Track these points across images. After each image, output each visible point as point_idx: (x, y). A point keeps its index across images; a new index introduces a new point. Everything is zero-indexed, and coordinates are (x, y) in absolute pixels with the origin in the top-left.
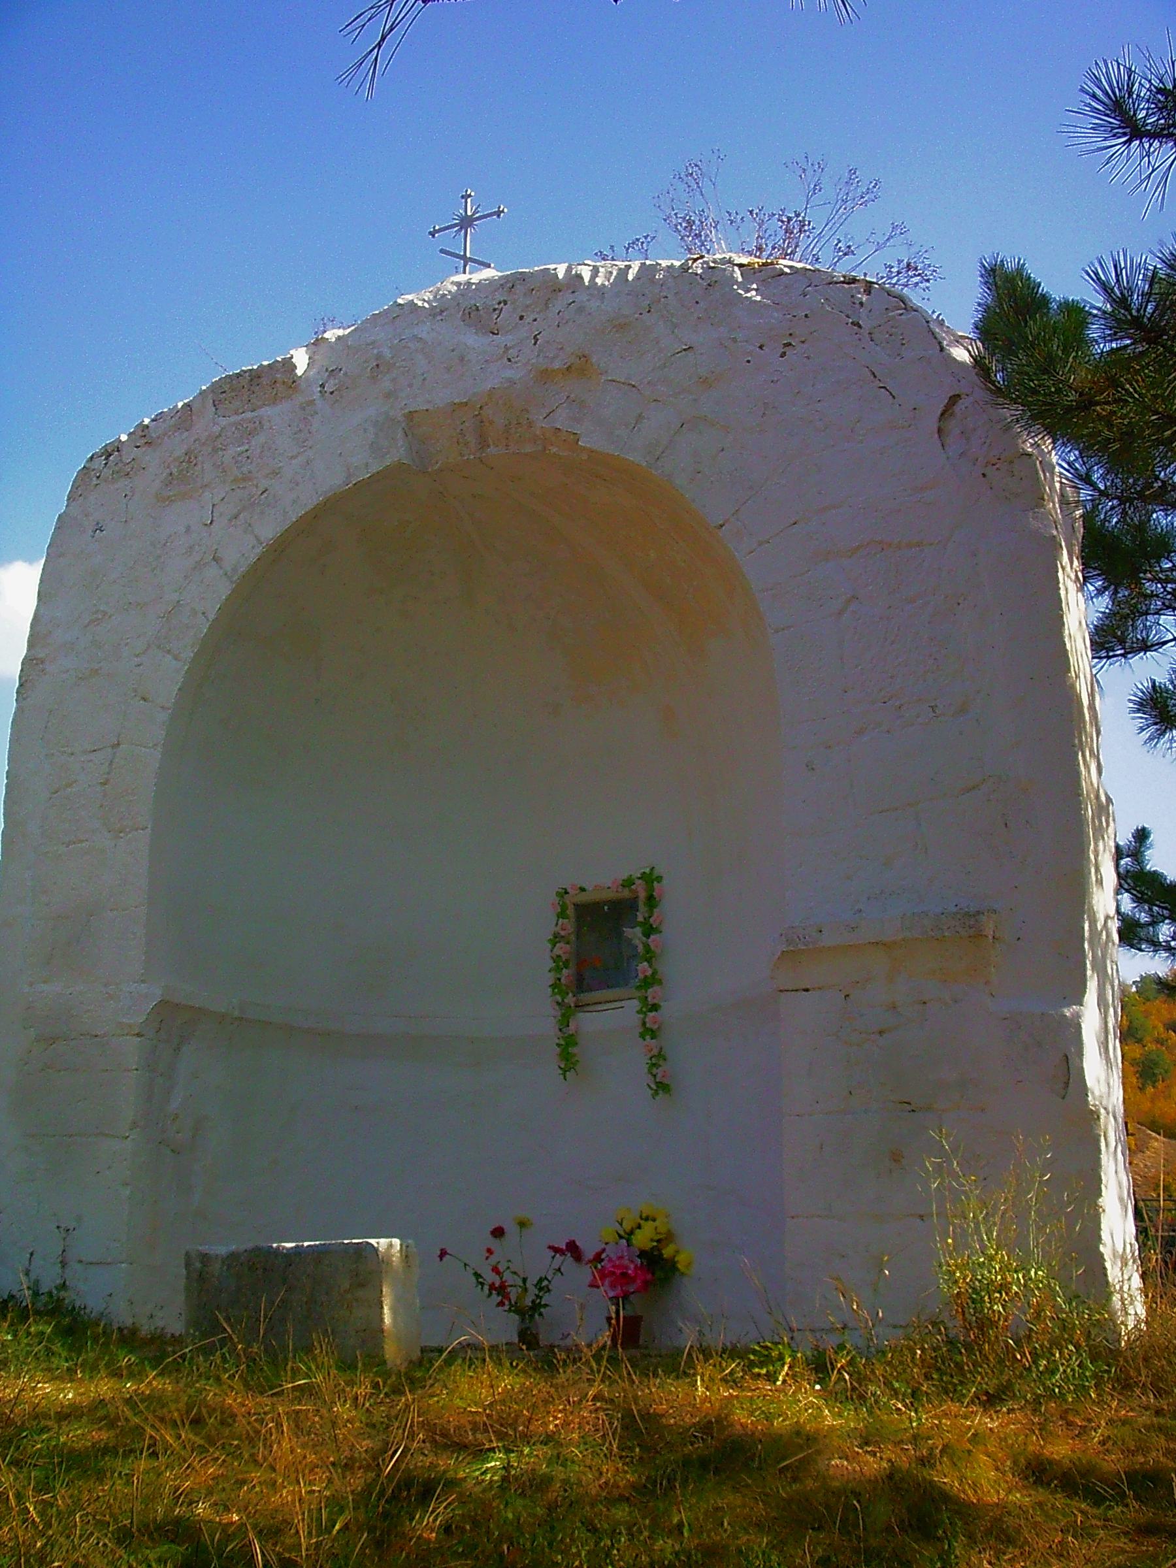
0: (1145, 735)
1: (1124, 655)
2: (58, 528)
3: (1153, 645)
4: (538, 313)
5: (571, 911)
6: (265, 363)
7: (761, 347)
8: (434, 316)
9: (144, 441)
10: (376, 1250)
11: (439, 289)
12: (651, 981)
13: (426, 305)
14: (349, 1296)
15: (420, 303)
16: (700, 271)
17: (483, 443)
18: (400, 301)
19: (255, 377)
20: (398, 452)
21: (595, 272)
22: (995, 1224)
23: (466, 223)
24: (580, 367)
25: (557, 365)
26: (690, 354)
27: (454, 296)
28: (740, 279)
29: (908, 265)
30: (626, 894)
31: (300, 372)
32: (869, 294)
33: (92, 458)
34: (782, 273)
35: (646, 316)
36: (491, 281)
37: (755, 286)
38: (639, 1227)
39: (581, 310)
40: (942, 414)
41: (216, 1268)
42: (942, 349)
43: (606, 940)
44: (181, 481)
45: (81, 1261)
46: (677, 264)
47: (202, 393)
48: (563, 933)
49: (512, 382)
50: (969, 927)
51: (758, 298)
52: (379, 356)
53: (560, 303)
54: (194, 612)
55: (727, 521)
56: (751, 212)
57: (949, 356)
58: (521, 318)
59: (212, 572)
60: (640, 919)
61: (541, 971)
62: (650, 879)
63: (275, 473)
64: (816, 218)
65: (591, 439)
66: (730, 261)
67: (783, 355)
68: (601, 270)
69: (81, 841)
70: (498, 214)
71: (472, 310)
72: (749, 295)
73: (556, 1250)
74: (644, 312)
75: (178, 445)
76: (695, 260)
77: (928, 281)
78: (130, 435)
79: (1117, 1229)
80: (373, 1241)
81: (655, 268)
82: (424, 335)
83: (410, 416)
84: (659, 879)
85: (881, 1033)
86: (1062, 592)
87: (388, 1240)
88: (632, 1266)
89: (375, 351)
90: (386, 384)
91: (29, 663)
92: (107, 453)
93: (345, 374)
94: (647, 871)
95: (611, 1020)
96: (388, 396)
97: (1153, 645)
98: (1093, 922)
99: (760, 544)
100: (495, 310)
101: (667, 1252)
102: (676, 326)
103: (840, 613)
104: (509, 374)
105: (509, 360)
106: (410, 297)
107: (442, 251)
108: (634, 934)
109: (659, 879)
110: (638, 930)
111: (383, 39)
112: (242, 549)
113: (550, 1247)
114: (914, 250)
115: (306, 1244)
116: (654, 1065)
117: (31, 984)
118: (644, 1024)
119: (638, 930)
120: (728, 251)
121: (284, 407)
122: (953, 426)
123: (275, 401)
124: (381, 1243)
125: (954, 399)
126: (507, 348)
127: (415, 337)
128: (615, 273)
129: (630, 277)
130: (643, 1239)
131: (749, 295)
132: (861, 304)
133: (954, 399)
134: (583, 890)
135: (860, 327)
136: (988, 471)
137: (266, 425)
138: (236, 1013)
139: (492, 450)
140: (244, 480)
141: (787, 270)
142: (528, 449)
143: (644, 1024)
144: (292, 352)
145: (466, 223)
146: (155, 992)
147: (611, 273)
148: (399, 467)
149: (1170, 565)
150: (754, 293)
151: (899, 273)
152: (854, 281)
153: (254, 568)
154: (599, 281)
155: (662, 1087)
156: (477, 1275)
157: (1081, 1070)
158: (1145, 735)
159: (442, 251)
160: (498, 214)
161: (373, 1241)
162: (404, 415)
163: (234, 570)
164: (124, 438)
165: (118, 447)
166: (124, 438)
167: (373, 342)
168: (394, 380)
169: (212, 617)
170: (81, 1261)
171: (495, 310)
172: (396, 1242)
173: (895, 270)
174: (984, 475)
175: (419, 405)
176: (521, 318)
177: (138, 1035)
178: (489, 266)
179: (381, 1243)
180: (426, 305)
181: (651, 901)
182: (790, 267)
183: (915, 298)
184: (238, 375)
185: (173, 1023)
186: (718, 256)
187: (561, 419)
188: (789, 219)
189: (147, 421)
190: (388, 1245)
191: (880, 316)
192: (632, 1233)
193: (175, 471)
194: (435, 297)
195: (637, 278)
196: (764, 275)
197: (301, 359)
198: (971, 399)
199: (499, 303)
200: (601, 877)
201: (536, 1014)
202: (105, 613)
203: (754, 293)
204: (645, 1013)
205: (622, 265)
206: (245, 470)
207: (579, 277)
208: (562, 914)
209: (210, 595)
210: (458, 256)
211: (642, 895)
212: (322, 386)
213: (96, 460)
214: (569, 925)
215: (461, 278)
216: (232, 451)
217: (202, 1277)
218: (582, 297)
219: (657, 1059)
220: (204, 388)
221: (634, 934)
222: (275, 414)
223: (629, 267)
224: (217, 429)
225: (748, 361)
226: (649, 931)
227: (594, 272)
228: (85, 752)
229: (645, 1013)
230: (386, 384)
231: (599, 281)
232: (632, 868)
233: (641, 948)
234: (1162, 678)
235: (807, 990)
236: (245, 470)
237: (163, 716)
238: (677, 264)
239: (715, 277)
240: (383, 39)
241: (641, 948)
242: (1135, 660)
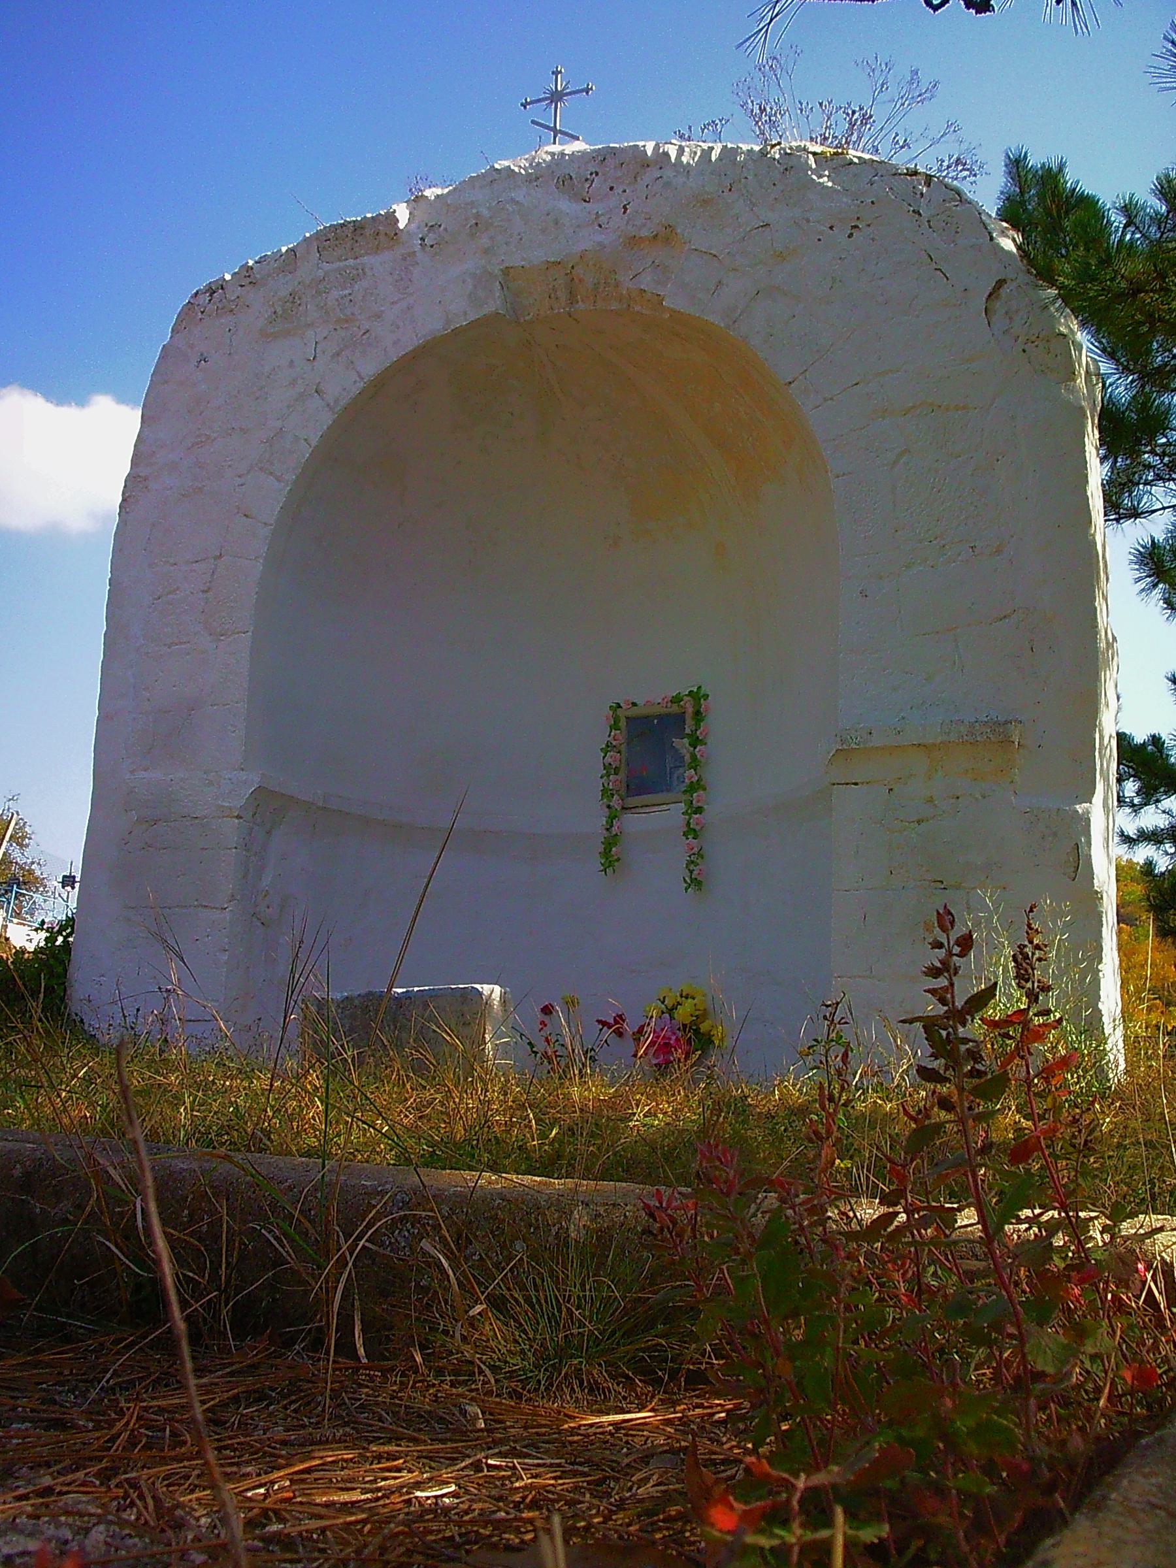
0: (1142, 585)
1: (1117, 520)
2: (163, 357)
3: (1143, 513)
5: (623, 723)
6: (369, 215)
7: (831, 228)
8: (530, 182)
9: (249, 280)
10: (481, 994)
11: (534, 158)
12: (695, 787)
13: (523, 172)
15: (516, 169)
16: (777, 156)
17: (572, 299)
18: (497, 166)
19: (358, 228)
20: (494, 304)
21: (681, 150)
22: (507, 1513)
23: (556, 97)
24: (666, 236)
25: (644, 233)
27: (549, 166)
28: (814, 166)
29: (958, 159)
30: (675, 709)
31: (401, 225)
32: (929, 186)
33: (196, 294)
34: (851, 163)
36: (584, 153)
37: (827, 173)
38: (679, 1004)
39: (667, 185)
40: (990, 296)
42: (992, 239)
43: (655, 749)
44: (285, 318)
46: (757, 148)
47: (306, 239)
48: (614, 743)
50: (997, 736)
51: (830, 184)
52: (478, 215)
53: (649, 176)
54: (297, 438)
56: (821, 104)
57: (998, 244)
58: (612, 189)
59: (316, 402)
60: (688, 731)
61: (594, 777)
63: (378, 316)
64: (879, 114)
65: (674, 301)
66: (805, 149)
67: (850, 236)
68: (687, 149)
69: (181, 643)
70: (587, 91)
71: (564, 177)
72: (821, 180)
73: (604, 1023)
74: (726, 190)
76: (773, 146)
77: (975, 175)
78: (234, 275)
79: (1110, 1000)
80: (478, 986)
81: (736, 151)
82: (520, 198)
83: (506, 271)
84: (706, 696)
85: (919, 822)
86: (1087, 455)
87: (491, 986)
88: (674, 1038)
89: (474, 211)
90: (485, 241)
91: (132, 482)
92: (211, 291)
93: (446, 230)
95: (656, 822)
96: (486, 251)
97: (1143, 513)
98: (1102, 738)
99: (825, 400)
100: (587, 180)
101: (704, 1027)
103: (895, 463)
104: (601, 238)
105: (600, 226)
106: (506, 163)
107: (533, 122)
108: (682, 745)
109: (706, 696)
110: (686, 741)
111: (771, 20)
112: (345, 382)
113: (599, 1021)
114: (964, 146)
115: (416, 989)
116: (693, 862)
117: (132, 772)
118: (688, 824)
119: (686, 741)
120: (793, 138)
121: (387, 256)
122: (998, 306)
123: (377, 250)
124: (485, 989)
125: (1000, 283)
127: (513, 200)
128: (699, 154)
129: (713, 159)
130: (684, 1013)
131: (821, 180)
132: (922, 194)
133: (1000, 283)
134: (634, 704)
135: (920, 214)
136: (1026, 347)
137: (369, 273)
138: (320, 804)
139: (581, 306)
141: (856, 160)
142: (615, 306)
143: (688, 824)
144: (394, 207)
145: (556, 97)
146: (253, 779)
147: (695, 153)
149: (1164, 440)
150: (826, 179)
151: (949, 167)
152: (915, 173)
154: (684, 159)
155: (695, 883)
157: (1089, 857)
158: (1142, 585)
159: (533, 122)
160: (587, 91)
161: (478, 986)
163: (337, 401)
164: (228, 277)
165: (222, 285)
166: (228, 277)
167: (472, 202)
168: (492, 238)
169: (314, 444)
171: (587, 180)
172: (497, 989)
173: (945, 164)
174: (1024, 351)
175: (516, 261)
176: (612, 189)
177: (238, 817)
178: (578, 139)
179: (485, 989)
180: (523, 172)
182: (859, 158)
183: (965, 187)
184: (342, 225)
185: (268, 808)
186: (794, 144)
187: (647, 281)
188: (854, 112)
189: (251, 263)
190: (493, 991)
191: (927, 200)
192: (674, 1008)
193: (279, 310)
194: (531, 165)
195: (720, 159)
196: (836, 162)
197: (402, 214)
198: (1015, 284)
200: (652, 691)
202: (208, 437)
203: (826, 179)
204: (690, 815)
205: (705, 146)
206: (348, 312)
207: (666, 154)
208: (615, 726)
209: (311, 425)
210: (547, 127)
211: (690, 710)
212: (422, 239)
213: (201, 296)
214: (621, 736)
215: (556, 148)
216: (335, 294)
218: (668, 173)
219: (696, 858)
220: (308, 235)
221: (682, 745)
222: (379, 263)
223: (712, 148)
224: (321, 273)
226: (696, 742)
227: (684, 152)
229: (690, 815)
230: (485, 241)
231: (684, 159)
232: (684, 688)
233: (687, 758)
234: (1160, 537)
235: (856, 784)
236: (348, 312)
238: (757, 148)
239: (791, 162)
240: (771, 20)
241: (687, 758)
242: (1127, 524)
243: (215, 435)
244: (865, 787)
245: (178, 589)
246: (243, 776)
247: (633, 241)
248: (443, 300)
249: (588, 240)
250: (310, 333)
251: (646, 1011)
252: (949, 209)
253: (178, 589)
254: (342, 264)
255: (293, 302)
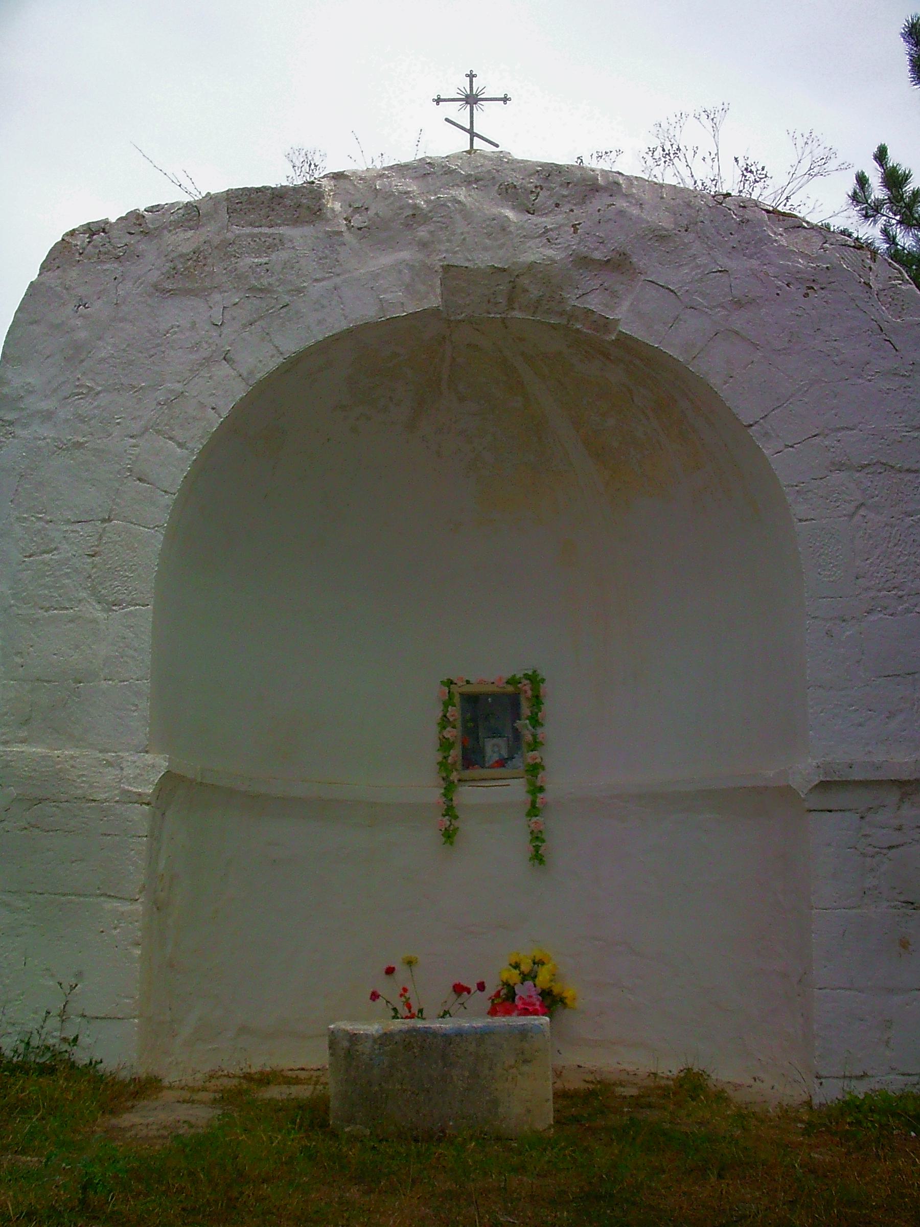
4: (575, 205)
5: (457, 699)
8: (470, 183)
14: (514, 1070)
24: (619, 263)
25: (597, 255)
26: (725, 275)
30: (510, 689)
35: (684, 234)
41: (365, 1048)
44: (186, 278)
45: (84, 1016)
49: (554, 261)
54: (202, 406)
55: (756, 422)
62: (534, 679)
75: (184, 241)
82: (462, 198)
83: (447, 268)
90: (422, 233)
94: (530, 673)
95: (493, 796)
102: (711, 248)
104: (550, 252)
109: (543, 680)
112: (260, 358)
121: (308, 230)
123: (296, 222)
126: (547, 230)
134: (468, 682)
135: (871, 287)
138: (199, 780)
140: (261, 290)
146: (159, 762)
148: (434, 313)
153: (271, 375)
155: (538, 857)
156: (395, 1009)
162: (442, 266)
163: (251, 373)
170: (84, 1016)
171: (532, 192)
175: (459, 260)
181: (537, 700)
187: (594, 303)
199: (536, 187)
200: (489, 670)
201: (416, 780)
202: (90, 389)
209: (220, 393)
214: (454, 712)
217: (350, 1054)
219: (537, 837)
225: (778, 294)
228: (68, 522)
235: (830, 811)
237: (168, 499)
243: (100, 388)
244: (840, 814)
245: (56, 549)
246: (149, 758)
247: (583, 262)
248: (380, 286)
249: (535, 253)
250: (217, 297)
251: (498, 974)
252: (894, 286)
253: (56, 549)
254: (256, 230)
255: (197, 261)
